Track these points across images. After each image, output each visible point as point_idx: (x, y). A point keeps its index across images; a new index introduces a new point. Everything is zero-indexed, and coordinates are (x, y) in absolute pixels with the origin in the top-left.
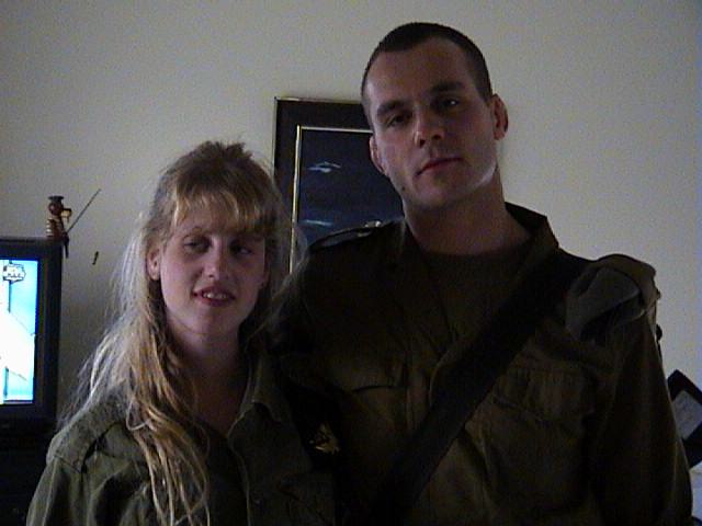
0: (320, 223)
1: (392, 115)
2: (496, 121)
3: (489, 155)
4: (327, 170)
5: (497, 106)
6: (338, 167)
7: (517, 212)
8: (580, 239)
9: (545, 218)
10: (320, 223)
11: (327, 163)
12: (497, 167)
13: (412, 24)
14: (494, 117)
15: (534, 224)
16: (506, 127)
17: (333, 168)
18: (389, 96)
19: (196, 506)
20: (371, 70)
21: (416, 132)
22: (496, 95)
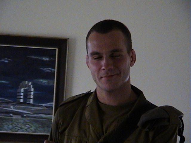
0: (4, 82)
1: (96, 56)
2: (132, 60)
3: (127, 73)
4: (6, 61)
5: (133, 53)
6: (11, 60)
7: (134, 89)
8: (156, 97)
9: (142, 92)
10: (4, 82)
11: (6, 59)
12: (130, 76)
13: (125, 26)
14: (131, 58)
15: (138, 92)
16: (134, 62)
17: (9, 60)
18: (95, 50)
19: (106, 133)
20: (90, 36)
21: (103, 62)
22: (133, 50)
